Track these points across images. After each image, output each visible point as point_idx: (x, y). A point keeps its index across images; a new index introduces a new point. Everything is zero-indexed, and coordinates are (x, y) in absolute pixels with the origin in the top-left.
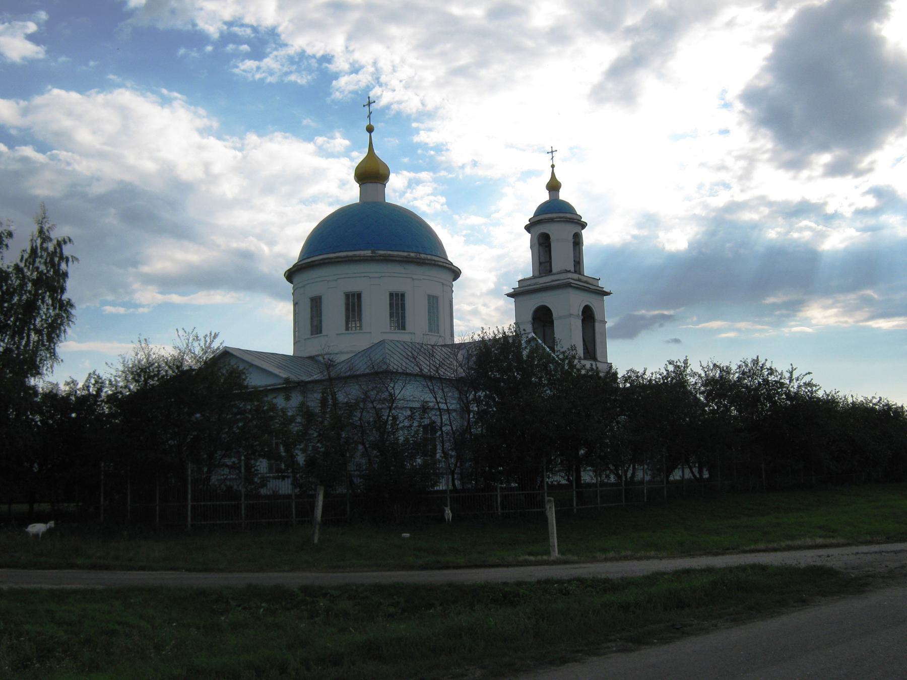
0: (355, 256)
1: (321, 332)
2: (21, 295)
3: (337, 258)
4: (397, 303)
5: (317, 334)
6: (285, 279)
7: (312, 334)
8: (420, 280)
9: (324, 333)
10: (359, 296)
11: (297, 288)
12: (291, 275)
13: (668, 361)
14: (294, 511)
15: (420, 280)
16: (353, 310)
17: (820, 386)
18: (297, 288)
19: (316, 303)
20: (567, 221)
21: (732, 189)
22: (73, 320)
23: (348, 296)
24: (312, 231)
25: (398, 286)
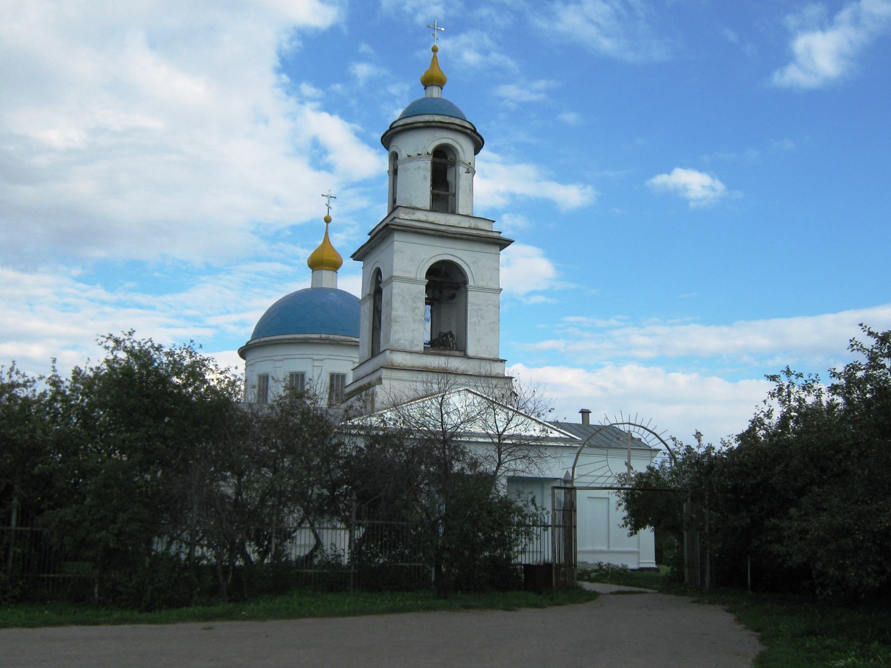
3: (294, 339)
11: (248, 365)
18: (248, 365)
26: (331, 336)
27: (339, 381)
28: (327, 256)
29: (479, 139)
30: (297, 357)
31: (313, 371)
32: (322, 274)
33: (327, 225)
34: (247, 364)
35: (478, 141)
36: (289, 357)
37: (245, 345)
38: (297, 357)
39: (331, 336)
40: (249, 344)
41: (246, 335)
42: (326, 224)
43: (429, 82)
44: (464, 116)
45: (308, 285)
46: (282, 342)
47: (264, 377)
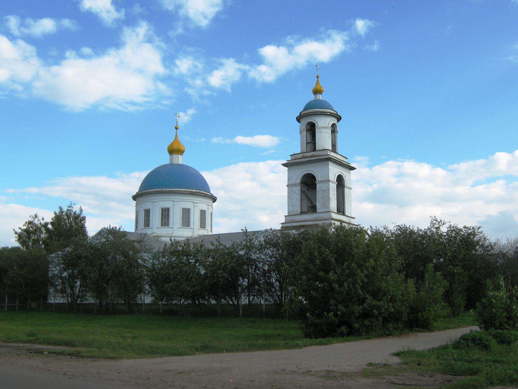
0: (179, 191)
1: (149, 226)
2: (163, 271)
3: (184, 191)
4: (186, 213)
5: (147, 227)
6: (132, 199)
7: (144, 227)
8: (198, 203)
9: (171, 225)
10: (149, 210)
11: (137, 204)
12: (135, 198)
13: (430, 222)
14: (11, 304)
15: (198, 203)
16: (165, 216)
17: (430, 225)
18: (137, 204)
19: (147, 212)
20: (190, 194)
21: (60, 206)
22: (140, 239)
23: (184, 210)
24: (145, 178)
25: (187, 205)
26: (164, 189)
27: (166, 212)
28: (175, 147)
29: (339, 117)
30: (186, 200)
31: (194, 208)
32: (173, 156)
33: (176, 131)
34: (137, 204)
35: (339, 118)
36: (202, 202)
37: (135, 194)
38: (186, 200)
39: (164, 189)
40: (137, 194)
41: (135, 189)
42: (176, 130)
43: (317, 92)
44: (333, 109)
45: (167, 162)
46: (180, 192)
47: (147, 210)
